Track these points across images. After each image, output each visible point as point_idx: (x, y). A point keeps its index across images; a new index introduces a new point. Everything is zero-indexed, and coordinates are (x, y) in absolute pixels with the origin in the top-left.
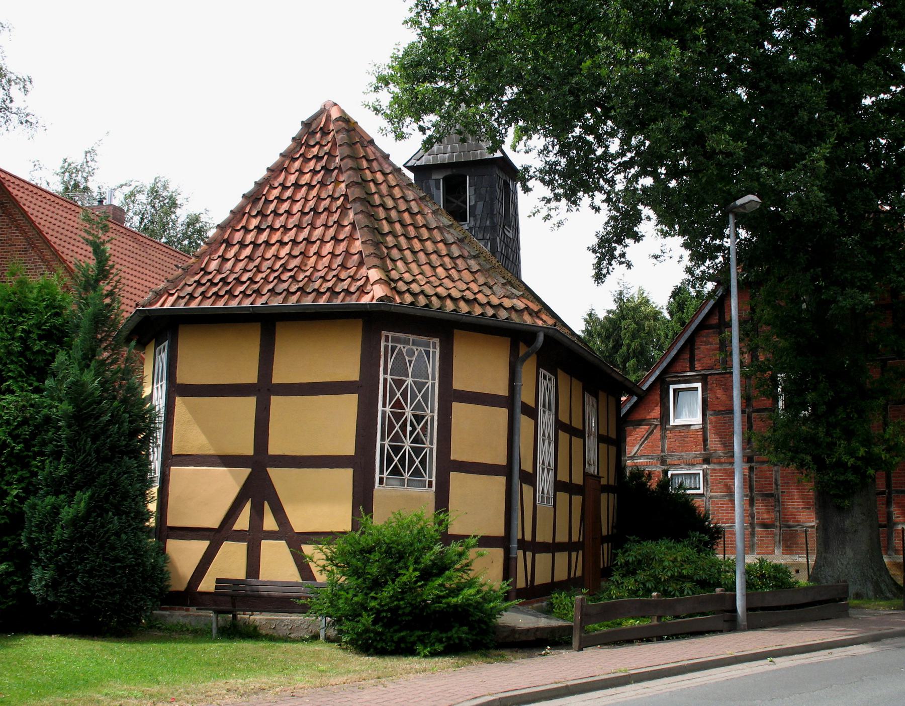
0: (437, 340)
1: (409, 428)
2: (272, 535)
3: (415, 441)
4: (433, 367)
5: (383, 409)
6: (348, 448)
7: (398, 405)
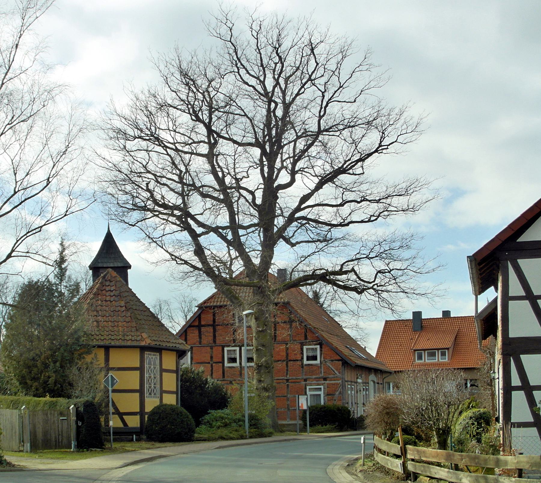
0: (158, 354)
1: (153, 381)
2: (517, 388)
3: (151, 377)
4: (158, 362)
5: (146, 375)
6: (138, 388)
7: (150, 374)
